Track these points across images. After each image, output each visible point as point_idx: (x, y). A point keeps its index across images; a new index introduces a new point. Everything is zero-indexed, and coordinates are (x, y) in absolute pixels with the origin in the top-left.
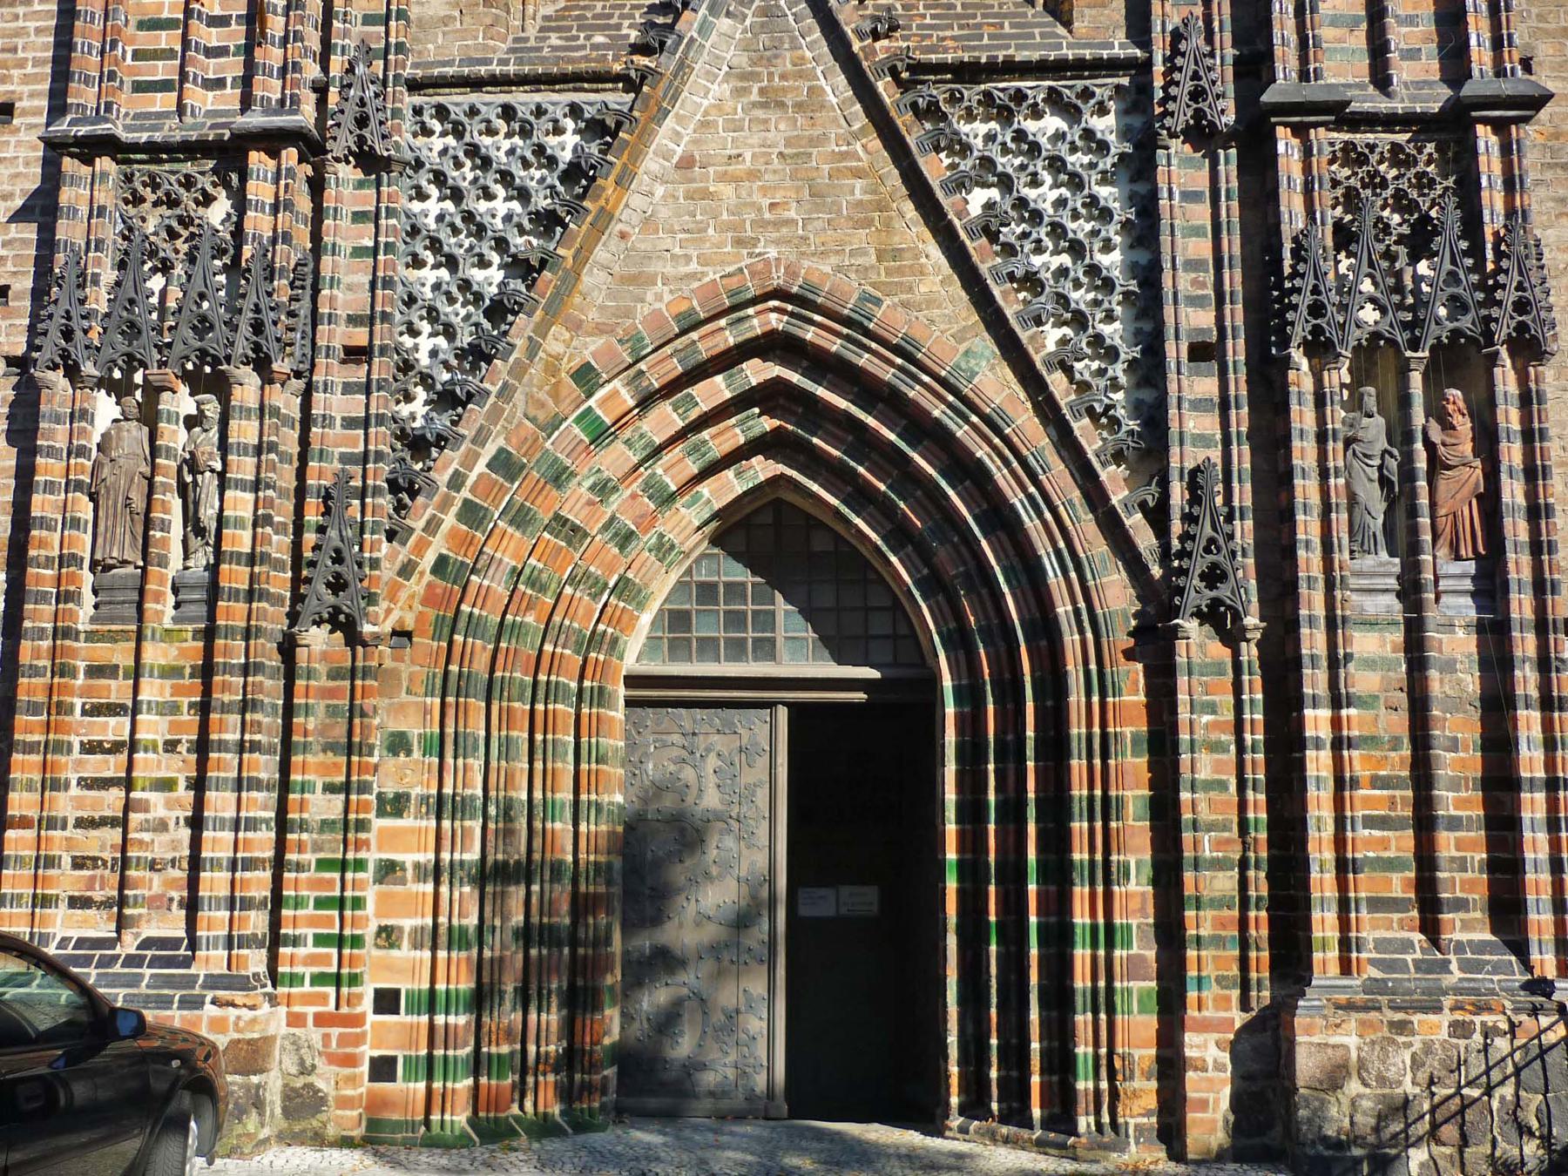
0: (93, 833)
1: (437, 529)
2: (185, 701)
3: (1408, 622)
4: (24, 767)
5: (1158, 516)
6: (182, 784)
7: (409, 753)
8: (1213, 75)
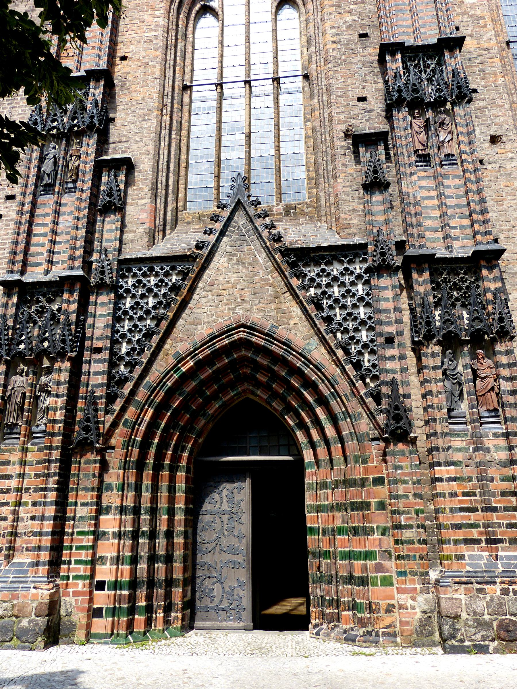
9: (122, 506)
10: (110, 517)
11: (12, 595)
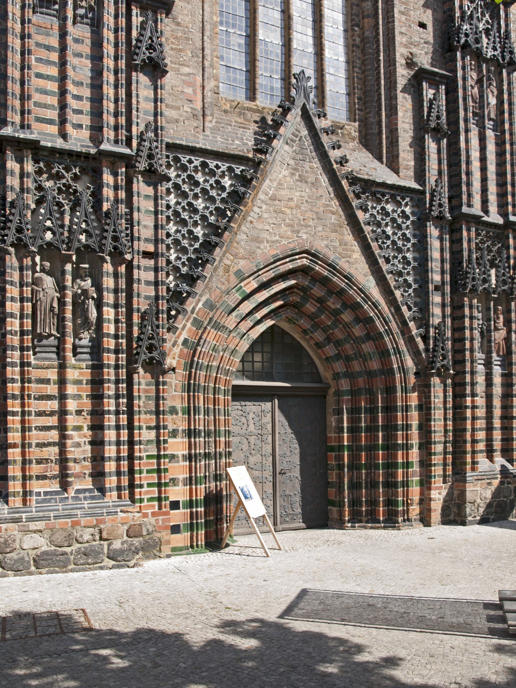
0: (44, 449)
1: (185, 329)
2: (84, 394)
3: (487, 373)
4: (14, 422)
5: (425, 338)
6: (86, 428)
7: (177, 414)
8: (157, 150)
9: (189, 430)
10: (179, 440)
11: (97, 520)
